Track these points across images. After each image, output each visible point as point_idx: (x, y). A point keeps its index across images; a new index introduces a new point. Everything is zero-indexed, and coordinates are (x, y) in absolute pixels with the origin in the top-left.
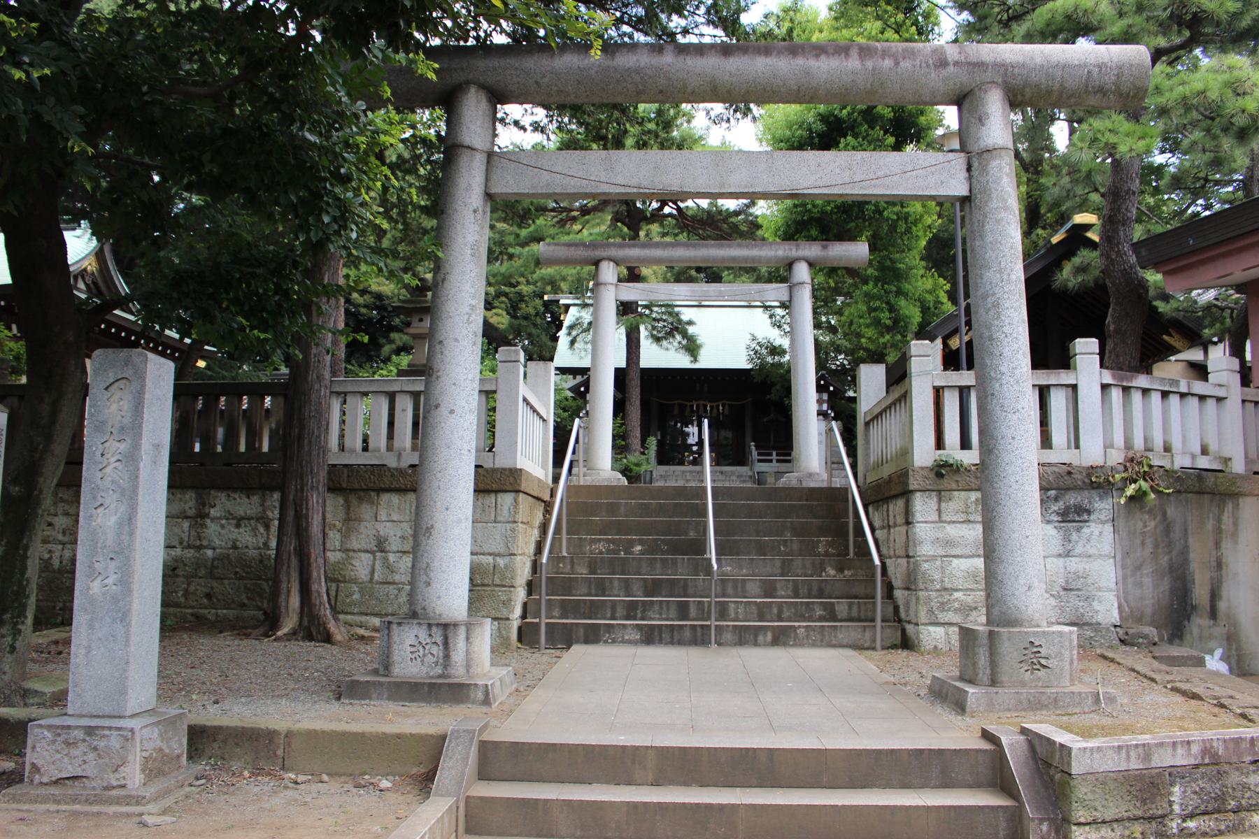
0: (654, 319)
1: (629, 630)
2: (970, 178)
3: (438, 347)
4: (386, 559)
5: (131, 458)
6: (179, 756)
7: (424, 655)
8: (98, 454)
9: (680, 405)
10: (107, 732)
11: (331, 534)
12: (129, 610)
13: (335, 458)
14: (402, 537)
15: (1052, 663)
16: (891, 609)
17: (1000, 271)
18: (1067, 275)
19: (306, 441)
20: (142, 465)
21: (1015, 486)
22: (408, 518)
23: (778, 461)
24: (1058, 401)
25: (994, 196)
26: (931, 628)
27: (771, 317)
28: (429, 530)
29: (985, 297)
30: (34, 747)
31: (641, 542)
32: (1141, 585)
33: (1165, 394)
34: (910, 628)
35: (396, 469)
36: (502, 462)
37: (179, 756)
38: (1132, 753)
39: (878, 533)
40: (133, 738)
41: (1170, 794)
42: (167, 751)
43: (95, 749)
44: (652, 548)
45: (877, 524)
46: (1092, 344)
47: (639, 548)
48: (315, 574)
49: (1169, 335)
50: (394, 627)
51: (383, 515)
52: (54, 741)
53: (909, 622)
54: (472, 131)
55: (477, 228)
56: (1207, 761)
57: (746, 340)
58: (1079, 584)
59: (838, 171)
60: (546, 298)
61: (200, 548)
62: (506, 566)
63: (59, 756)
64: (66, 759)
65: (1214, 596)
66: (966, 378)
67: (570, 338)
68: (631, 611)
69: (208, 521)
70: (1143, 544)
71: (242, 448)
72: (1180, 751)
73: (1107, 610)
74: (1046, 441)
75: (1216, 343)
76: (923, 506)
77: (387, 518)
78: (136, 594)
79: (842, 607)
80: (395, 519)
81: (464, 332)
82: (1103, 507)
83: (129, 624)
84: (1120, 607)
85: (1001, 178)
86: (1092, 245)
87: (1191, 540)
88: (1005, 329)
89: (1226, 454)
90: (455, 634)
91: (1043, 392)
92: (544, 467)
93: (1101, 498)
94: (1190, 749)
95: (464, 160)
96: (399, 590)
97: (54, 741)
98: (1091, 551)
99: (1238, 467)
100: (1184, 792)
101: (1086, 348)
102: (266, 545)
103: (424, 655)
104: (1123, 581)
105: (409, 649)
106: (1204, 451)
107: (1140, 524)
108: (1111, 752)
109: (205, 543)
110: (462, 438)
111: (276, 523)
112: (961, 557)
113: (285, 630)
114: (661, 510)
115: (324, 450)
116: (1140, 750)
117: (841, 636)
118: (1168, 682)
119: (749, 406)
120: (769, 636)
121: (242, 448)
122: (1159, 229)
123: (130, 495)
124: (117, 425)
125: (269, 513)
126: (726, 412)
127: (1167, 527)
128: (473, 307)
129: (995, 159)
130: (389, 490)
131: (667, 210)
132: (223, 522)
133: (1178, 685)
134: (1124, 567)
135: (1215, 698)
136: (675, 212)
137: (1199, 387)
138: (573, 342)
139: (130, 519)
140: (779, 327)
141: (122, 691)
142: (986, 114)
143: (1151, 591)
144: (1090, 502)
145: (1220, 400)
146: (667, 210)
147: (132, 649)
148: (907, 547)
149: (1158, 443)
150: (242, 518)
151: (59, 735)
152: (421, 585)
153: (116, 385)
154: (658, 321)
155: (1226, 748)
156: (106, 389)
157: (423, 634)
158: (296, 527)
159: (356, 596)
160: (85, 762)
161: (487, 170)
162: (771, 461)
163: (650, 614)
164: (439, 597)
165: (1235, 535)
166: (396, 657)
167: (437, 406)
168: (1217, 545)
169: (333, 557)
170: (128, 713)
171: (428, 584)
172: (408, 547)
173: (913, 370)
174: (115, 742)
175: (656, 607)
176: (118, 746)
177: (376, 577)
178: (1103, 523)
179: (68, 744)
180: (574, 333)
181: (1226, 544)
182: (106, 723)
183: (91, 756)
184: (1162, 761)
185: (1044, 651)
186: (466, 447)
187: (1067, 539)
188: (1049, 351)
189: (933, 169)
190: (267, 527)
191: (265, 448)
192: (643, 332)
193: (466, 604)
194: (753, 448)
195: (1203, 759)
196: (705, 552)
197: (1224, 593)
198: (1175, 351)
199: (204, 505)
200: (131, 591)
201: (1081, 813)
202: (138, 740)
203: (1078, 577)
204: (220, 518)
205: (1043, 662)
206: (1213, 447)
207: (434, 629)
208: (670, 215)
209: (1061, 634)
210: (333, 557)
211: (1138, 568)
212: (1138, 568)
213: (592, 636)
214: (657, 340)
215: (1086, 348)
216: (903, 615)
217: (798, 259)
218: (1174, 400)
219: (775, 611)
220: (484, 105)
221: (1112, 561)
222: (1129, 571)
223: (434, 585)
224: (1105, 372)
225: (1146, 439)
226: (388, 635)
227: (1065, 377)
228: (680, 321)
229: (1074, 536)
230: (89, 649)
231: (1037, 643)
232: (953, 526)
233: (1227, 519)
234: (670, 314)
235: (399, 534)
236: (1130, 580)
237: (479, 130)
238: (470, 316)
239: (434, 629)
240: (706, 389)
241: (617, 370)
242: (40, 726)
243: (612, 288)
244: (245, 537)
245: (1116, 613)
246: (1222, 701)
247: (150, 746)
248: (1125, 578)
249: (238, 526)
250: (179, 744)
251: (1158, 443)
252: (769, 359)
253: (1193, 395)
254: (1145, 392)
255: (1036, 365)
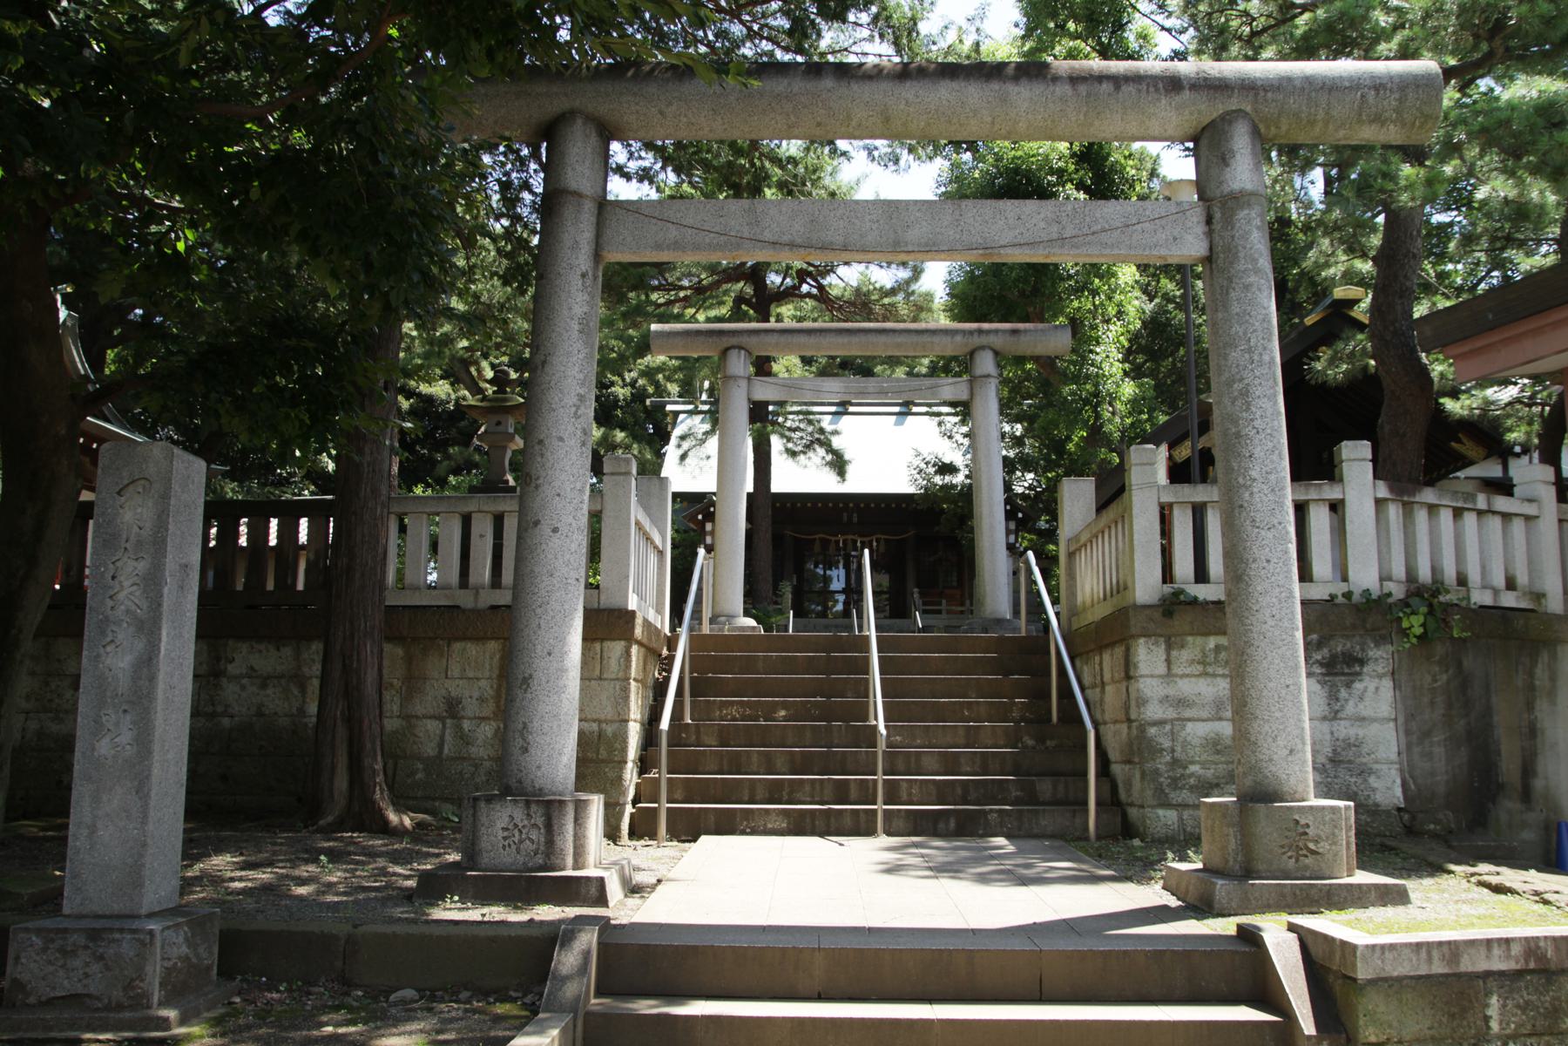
0: (790, 429)
1: (773, 817)
2: (1210, 234)
3: (537, 448)
4: (459, 727)
5: (152, 582)
6: (209, 968)
7: (521, 841)
8: (108, 576)
9: (822, 540)
10: (117, 936)
11: (387, 696)
12: (148, 777)
13: (392, 600)
14: (481, 700)
15: (1323, 847)
16: (1107, 788)
17: (1250, 351)
18: (1328, 367)
19: (358, 575)
20: (166, 590)
21: (1271, 622)
22: (487, 674)
23: (948, 612)
24: (1319, 519)
25: (1241, 255)
26: (1161, 812)
27: (940, 424)
28: (527, 681)
29: (1229, 384)
30: (17, 958)
31: (785, 705)
32: (1429, 756)
33: (1458, 513)
34: (1133, 813)
35: (473, 611)
36: (607, 600)
37: (209, 968)
38: (1435, 953)
39: (1088, 692)
40: (152, 943)
41: (1487, 1006)
42: (194, 960)
43: (101, 958)
44: (798, 713)
45: (1087, 681)
46: (1364, 448)
47: (783, 713)
48: (369, 746)
49: (1459, 441)
50: (482, 804)
51: (455, 671)
52: (45, 950)
53: (1132, 805)
54: (578, 176)
55: (586, 297)
56: (1532, 965)
57: (909, 456)
58: (1350, 755)
59: (1042, 225)
60: (648, 402)
61: (213, 715)
62: (615, 735)
63: (51, 968)
64: (61, 973)
65: (1528, 770)
66: (1199, 493)
67: (681, 452)
68: (775, 793)
69: (225, 680)
70: (1432, 703)
71: (270, 586)
72: (1496, 951)
73: (1389, 789)
74: (1305, 575)
75: (1518, 455)
76: (1149, 657)
77: (464, 672)
78: (156, 757)
79: (1045, 787)
80: (471, 675)
81: (571, 429)
82: (1380, 657)
83: (148, 796)
84: (1404, 785)
85: (1249, 233)
86: (1360, 326)
87: (1494, 699)
88: (1256, 423)
89: (1538, 588)
90: (562, 814)
91: (1301, 509)
92: (659, 611)
93: (1377, 645)
94: (1509, 949)
95: (568, 212)
96: (476, 766)
97: (45, 950)
98: (1365, 713)
99: (1555, 604)
100: (1504, 1006)
101: (1356, 456)
102: (302, 711)
103: (521, 841)
104: (1407, 749)
105: (501, 834)
106: (1511, 585)
107: (1428, 678)
108: (1407, 951)
109: (220, 709)
110: (568, 564)
111: (316, 682)
112: (1198, 720)
113: (330, 819)
114: (810, 665)
115: (382, 585)
116: (1445, 949)
117: (1044, 823)
118: (1473, 875)
119: (920, 537)
120: (952, 824)
121: (270, 586)
122: (1443, 304)
123: (149, 627)
124: (133, 538)
125: (305, 670)
126: (882, 549)
127: (1463, 681)
128: (581, 398)
129: (1242, 208)
130: (464, 638)
131: (805, 288)
132: (245, 681)
133: (1486, 878)
134: (1408, 733)
135: (1536, 893)
136: (815, 291)
137: (1502, 503)
138: (683, 457)
139: (150, 659)
140: (950, 437)
141: (138, 884)
142: (1232, 151)
143: (1441, 765)
144: (1363, 650)
145: (1528, 518)
146: (805, 288)
147: (150, 827)
148: (1127, 708)
149: (1450, 573)
150: (269, 677)
151: (53, 941)
152: (516, 751)
153: (131, 488)
154: (794, 430)
155: (1557, 948)
156: (119, 493)
157: (519, 814)
158: (344, 686)
159: (419, 776)
160: (86, 975)
161: (598, 224)
162: (939, 612)
163: (799, 795)
164: (539, 767)
165: (1552, 694)
166: (484, 843)
167: (537, 523)
168: (1530, 706)
169: (391, 724)
170: (143, 911)
171: (525, 750)
172: (488, 710)
173: (1134, 481)
174: (127, 948)
175: (808, 788)
176: (132, 954)
177: (446, 751)
178: (1380, 677)
179: (64, 952)
180: (686, 445)
181: (1542, 705)
182: (117, 924)
183: (95, 968)
184: (1473, 964)
185: (1311, 831)
186: (573, 575)
187: (1333, 697)
188: (1312, 460)
189: (1163, 222)
190: (303, 690)
191: (300, 586)
192: (776, 443)
193: (573, 776)
194: (916, 596)
195: (1527, 962)
196: (866, 719)
197: (1540, 768)
198: (1469, 463)
199: (218, 659)
200: (150, 752)
201: (1371, 1030)
202: (158, 945)
203: (1348, 744)
204: (241, 676)
205: (1311, 846)
206: (1522, 579)
207: (534, 807)
208: (809, 295)
209: (1334, 809)
210: (391, 724)
211: (1427, 734)
212: (1427, 734)
213: (726, 826)
214: (793, 454)
215: (1356, 456)
216: (1123, 796)
217: (983, 348)
218: (1470, 519)
219: (959, 791)
220: (594, 140)
221: (1392, 725)
222: (1414, 738)
223: (532, 751)
224: (1381, 483)
225: (1434, 569)
226: (474, 815)
227: (1333, 493)
228: (822, 431)
229: (1343, 693)
230: (93, 829)
231: (1303, 822)
232: (1186, 680)
233: (1541, 672)
234: (810, 422)
235: (476, 694)
236: (1416, 750)
237: (587, 172)
238: (578, 408)
239: (534, 807)
240: (855, 520)
241: (749, 495)
242: (27, 930)
243: (744, 383)
244: (275, 701)
245: (1398, 792)
246: (1546, 896)
247: (175, 952)
248: (1409, 746)
249: (264, 686)
250: (209, 955)
251: (1450, 573)
252: (938, 480)
253: (1494, 513)
254: (1432, 509)
255: (1295, 477)
